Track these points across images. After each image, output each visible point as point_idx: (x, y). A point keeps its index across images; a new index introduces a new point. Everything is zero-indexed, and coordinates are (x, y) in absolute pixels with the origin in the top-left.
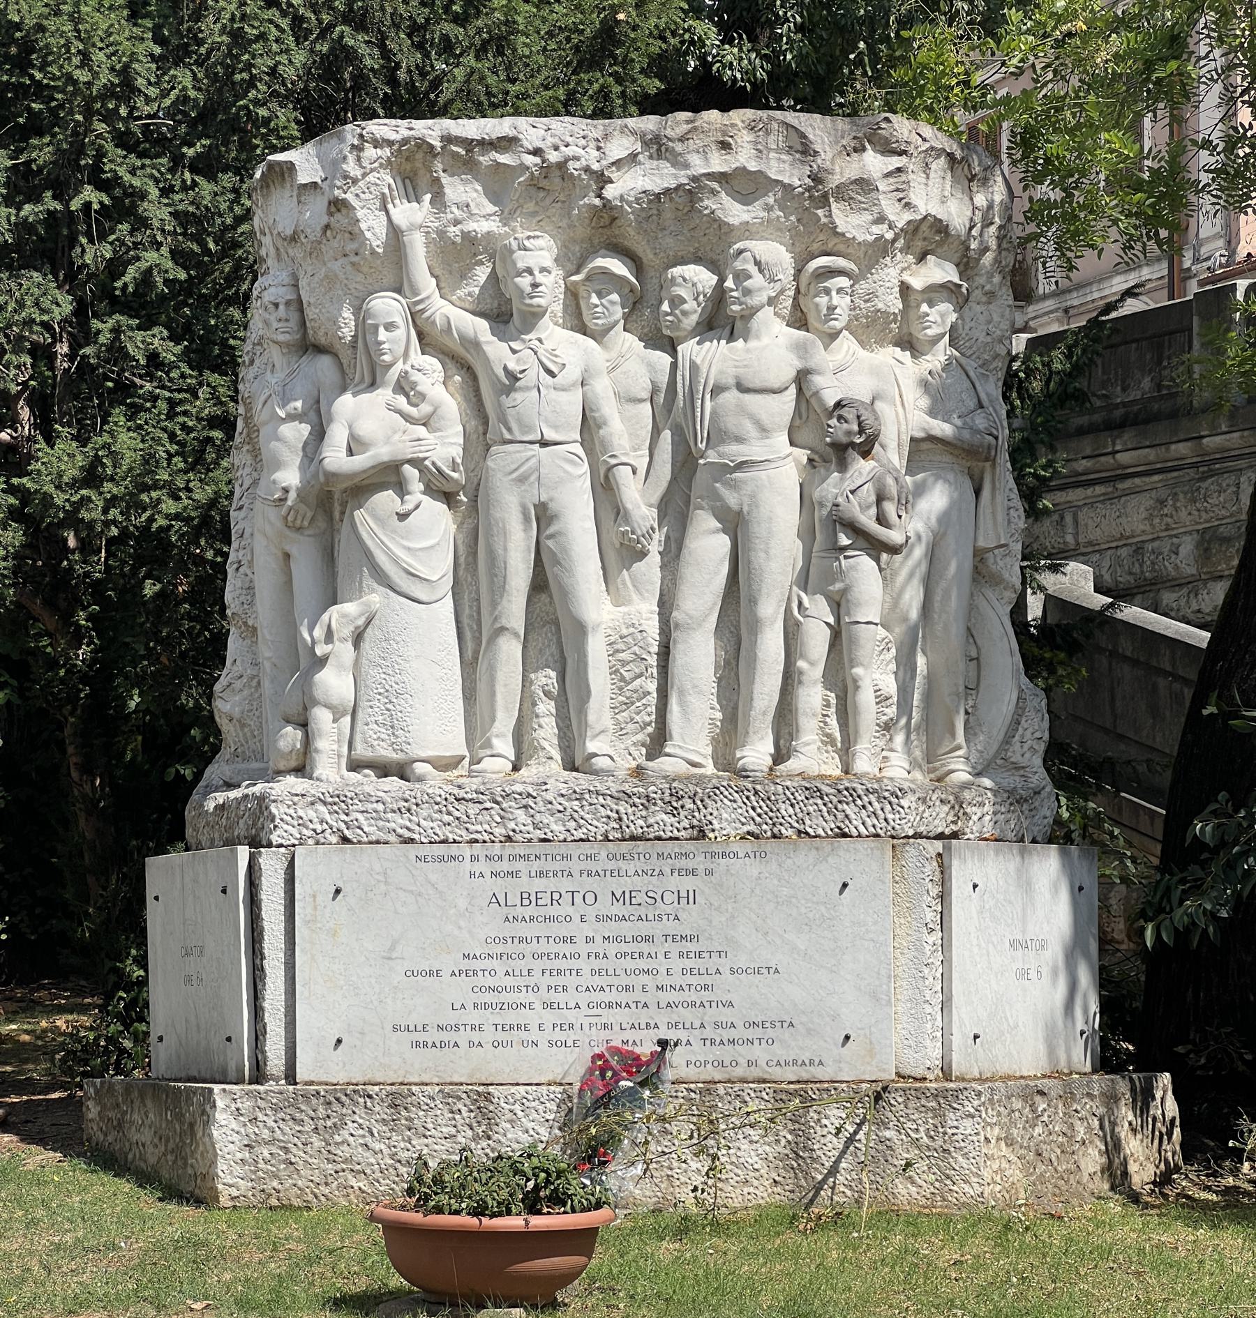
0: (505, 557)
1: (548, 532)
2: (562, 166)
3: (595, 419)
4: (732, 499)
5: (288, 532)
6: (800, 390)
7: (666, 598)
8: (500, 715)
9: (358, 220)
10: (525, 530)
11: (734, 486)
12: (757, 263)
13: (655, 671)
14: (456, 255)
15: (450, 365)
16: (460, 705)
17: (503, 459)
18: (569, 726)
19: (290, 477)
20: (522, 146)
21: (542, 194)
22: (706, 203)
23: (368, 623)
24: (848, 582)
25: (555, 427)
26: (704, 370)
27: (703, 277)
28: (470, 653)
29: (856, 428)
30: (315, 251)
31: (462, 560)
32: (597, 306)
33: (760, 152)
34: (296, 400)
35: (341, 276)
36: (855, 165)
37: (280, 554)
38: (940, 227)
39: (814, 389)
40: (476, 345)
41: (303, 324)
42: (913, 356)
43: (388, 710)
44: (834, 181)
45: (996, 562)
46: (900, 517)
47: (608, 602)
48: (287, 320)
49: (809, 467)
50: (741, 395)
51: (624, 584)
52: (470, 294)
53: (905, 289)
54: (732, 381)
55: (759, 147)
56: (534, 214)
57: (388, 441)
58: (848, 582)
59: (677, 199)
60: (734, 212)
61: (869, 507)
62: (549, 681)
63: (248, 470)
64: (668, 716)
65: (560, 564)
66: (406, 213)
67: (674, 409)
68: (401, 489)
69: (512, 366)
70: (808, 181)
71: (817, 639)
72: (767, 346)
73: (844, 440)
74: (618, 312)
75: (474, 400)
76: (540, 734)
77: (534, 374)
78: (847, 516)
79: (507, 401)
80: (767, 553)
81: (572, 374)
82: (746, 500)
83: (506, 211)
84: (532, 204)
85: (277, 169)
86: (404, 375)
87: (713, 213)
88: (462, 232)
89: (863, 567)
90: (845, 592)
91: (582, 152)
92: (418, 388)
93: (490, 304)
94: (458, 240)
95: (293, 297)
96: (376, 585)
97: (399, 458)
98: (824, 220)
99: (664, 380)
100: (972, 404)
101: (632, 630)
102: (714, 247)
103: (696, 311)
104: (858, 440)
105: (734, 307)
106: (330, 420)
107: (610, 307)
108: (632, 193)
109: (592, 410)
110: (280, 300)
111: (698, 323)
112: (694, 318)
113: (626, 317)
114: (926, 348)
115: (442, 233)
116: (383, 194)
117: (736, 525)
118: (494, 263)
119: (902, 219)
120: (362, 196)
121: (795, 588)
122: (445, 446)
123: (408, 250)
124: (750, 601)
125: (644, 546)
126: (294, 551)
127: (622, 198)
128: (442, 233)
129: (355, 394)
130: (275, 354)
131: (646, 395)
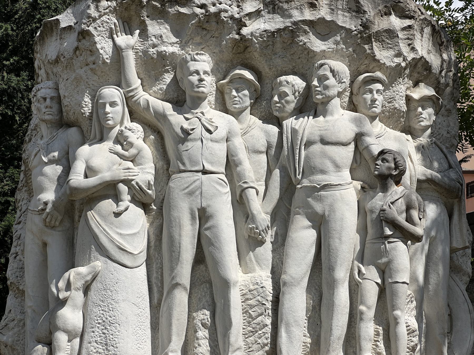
0: (180, 240)
1: (206, 226)
2: (217, 14)
3: (234, 161)
4: (318, 207)
5: (46, 229)
6: (356, 146)
7: (275, 269)
8: (174, 338)
9: (96, 43)
10: (192, 225)
11: (320, 199)
12: (332, 71)
13: (270, 312)
14: (153, 65)
15: (148, 130)
16: (149, 332)
17: (179, 182)
18: (217, 346)
19: (49, 196)
20: (194, 3)
21: (205, 32)
22: (301, 38)
23: (94, 279)
24: (390, 257)
25: (211, 163)
26: (301, 132)
27: (298, 83)
28: (156, 301)
29: (393, 165)
30: (69, 66)
31: (152, 244)
32: (235, 97)
33: (333, 10)
34: (54, 152)
35: (85, 77)
36: (385, 22)
37: (40, 243)
38: (427, 66)
39: (366, 145)
40: (163, 117)
41: (61, 111)
42: (413, 138)
43: (104, 333)
44: (375, 28)
45: (458, 259)
46: (420, 219)
47: (240, 271)
48: (51, 108)
49: (362, 192)
50: (323, 146)
51: (251, 260)
52: (161, 89)
53: (408, 99)
54: (317, 138)
55: (332, 7)
56: (199, 44)
57: (109, 169)
58: (390, 257)
59: (284, 35)
60: (318, 45)
61: (402, 213)
62: (205, 317)
63: (25, 201)
64: (279, 339)
65: (213, 245)
66: (123, 40)
67: (281, 157)
68: (117, 199)
69: (186, 125)
70: (360, 27)
71: (371, 292)
72: (338, 119)
73: (386, 172)
74: (248, 102)
75: (161, 150)
76: (200, 350)
77: (199, 131)
78: (390, 216)
79: (182, 148)
80: (340, 239)
81: (221, 133)
82: (327, 209)
83: (184, 41)
84: (199, 38)
85: (49, 25)
86: (121, 133)
87: (305, 44)
88: (157, 51)
89: (400, 251)
90: (389, 263)
91: (229, 8)
92: (129, 140)
93: (173, 95)
94: (155, 56)
95: (55, 95)
96: (99, 256)
97: (117, 179)
98: (368, 51)
99: (274, 140)
100: (446, 166)
101: (256, 286)
102: (305, 65)
103: (293, 102)
104: (394, 173)
105: (318, 97)
106: (75, 159)
107: (244, 98)
108: (258, 31)
109: (233, 156)
110: (47, 96)
111: (295, 109)
112: (292, 106)
113: (252, 106)
114: (420, 134)
115: (145, 52)
116: (111, 28)
117: (321, 223)
118: (175, 72)
119: (411, 57)
120: (99, 28)
121: (356, 262)
122: (145, 174)
123: (125, 61)
124: (329, 269)
125: (263, 237)
126: (49, 240)
127: (252, 34)
128: (145, 52)
129: (90, 145)
130: (44, 129)
131: (264, 149)
